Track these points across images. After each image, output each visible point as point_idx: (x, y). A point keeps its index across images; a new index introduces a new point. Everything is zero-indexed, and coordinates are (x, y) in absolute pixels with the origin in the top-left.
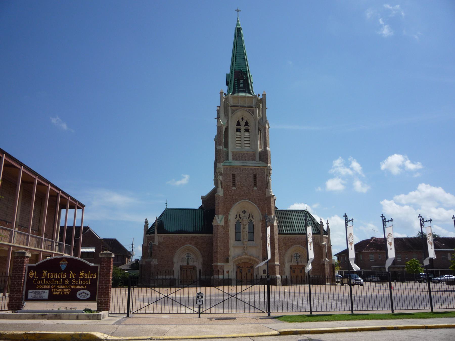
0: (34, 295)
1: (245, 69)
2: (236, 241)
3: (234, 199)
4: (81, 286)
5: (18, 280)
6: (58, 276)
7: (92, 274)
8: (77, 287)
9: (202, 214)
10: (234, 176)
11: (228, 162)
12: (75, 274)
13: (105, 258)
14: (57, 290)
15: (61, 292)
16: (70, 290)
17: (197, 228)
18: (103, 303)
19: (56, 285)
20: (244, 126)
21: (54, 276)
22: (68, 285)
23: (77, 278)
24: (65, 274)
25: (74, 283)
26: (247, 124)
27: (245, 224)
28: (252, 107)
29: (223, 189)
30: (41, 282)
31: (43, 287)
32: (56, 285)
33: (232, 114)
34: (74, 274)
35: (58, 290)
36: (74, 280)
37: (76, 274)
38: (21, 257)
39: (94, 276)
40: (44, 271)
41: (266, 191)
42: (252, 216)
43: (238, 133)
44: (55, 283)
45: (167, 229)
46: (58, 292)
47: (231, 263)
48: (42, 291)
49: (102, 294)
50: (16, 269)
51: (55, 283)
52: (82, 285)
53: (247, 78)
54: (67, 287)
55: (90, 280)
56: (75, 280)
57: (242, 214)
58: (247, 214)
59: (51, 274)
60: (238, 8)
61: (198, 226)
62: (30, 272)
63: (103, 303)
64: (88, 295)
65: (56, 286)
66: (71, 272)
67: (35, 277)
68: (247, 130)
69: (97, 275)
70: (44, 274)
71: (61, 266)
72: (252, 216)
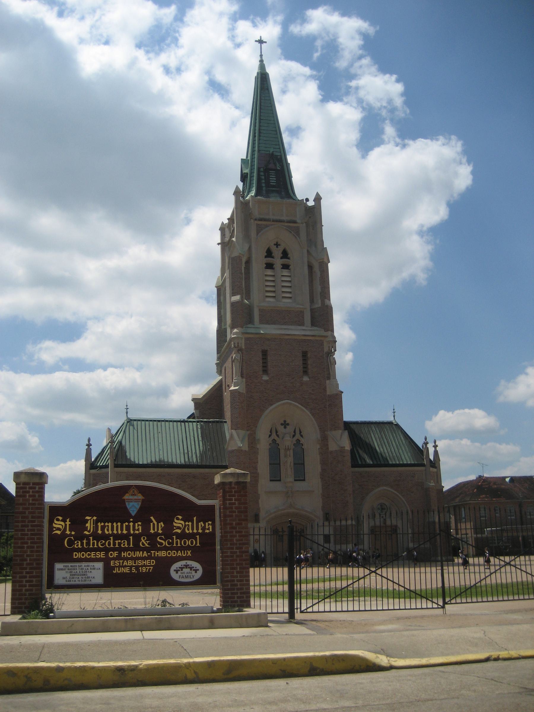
0: (68, 575)
1: (278, 150)
2: (271, 480)
3: (266, 400)
4: (179, 552)
5: (31, 539)
6: (122, 530)
7: (202, 523)
8: (169, 554)
9: (199, 430)
10: (265, 353)
11: (254, 328)
12: (162, 523)
13: (233, 486)
14: (123, 563)
15: (134, 566)
16: (153, 563)
17: (192, 456)
18: (238, 589)
19: (120, 550)
20: (279, 258)
21: (112, 529)
22: (148, 550)
23: (168, 534)
24: (140, 523)
25: (162, 544)
26: (285, 255)
27: (288, 448)
28: (295, 222)
29: (244, 380)
30: (82, 544)
31: (89, 555)
32: (120, 550)
33: (257, 235)
34: (160, 524)
35: (125, 561)
36: (161, 538)
37: (164, 524)
38: (34, 484)
39: (207, 527)
40: (88, 518)
41: (326, 383)
42: (300, 432)
43: (269, 272)
44: (117, 546)
45: (132, 459)
46: (126, 566)
47: (262, 524)
48: (88, 566)
49: (234, 569)
50: (25, 513)
51: (117, 546)
52: (182, 549)
53: (282, 166)
54: (145, 554)
55: (198, 537)
56: (163, 537)
57: (281, 429)
58: (290, 429)
59: (106, 524)
60: (261, 37)
61: (194, 452)
62: (56, 522)
63: (238, 589)
64: (196, 572)
65: (120, 553)
66: (152, 518)
67: (68, 532)
68: (286, 267)
69: (213, 525)
70: (88, 525)
71: (129, 505)
72: (300, 432)
